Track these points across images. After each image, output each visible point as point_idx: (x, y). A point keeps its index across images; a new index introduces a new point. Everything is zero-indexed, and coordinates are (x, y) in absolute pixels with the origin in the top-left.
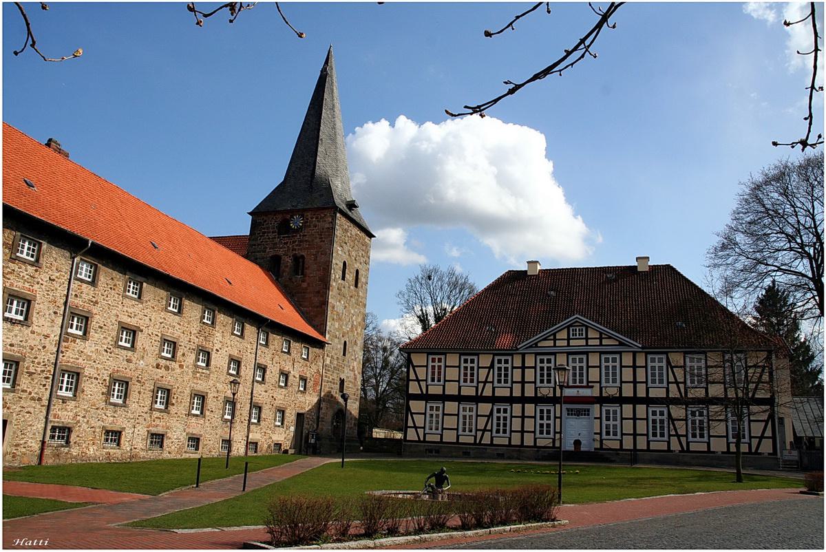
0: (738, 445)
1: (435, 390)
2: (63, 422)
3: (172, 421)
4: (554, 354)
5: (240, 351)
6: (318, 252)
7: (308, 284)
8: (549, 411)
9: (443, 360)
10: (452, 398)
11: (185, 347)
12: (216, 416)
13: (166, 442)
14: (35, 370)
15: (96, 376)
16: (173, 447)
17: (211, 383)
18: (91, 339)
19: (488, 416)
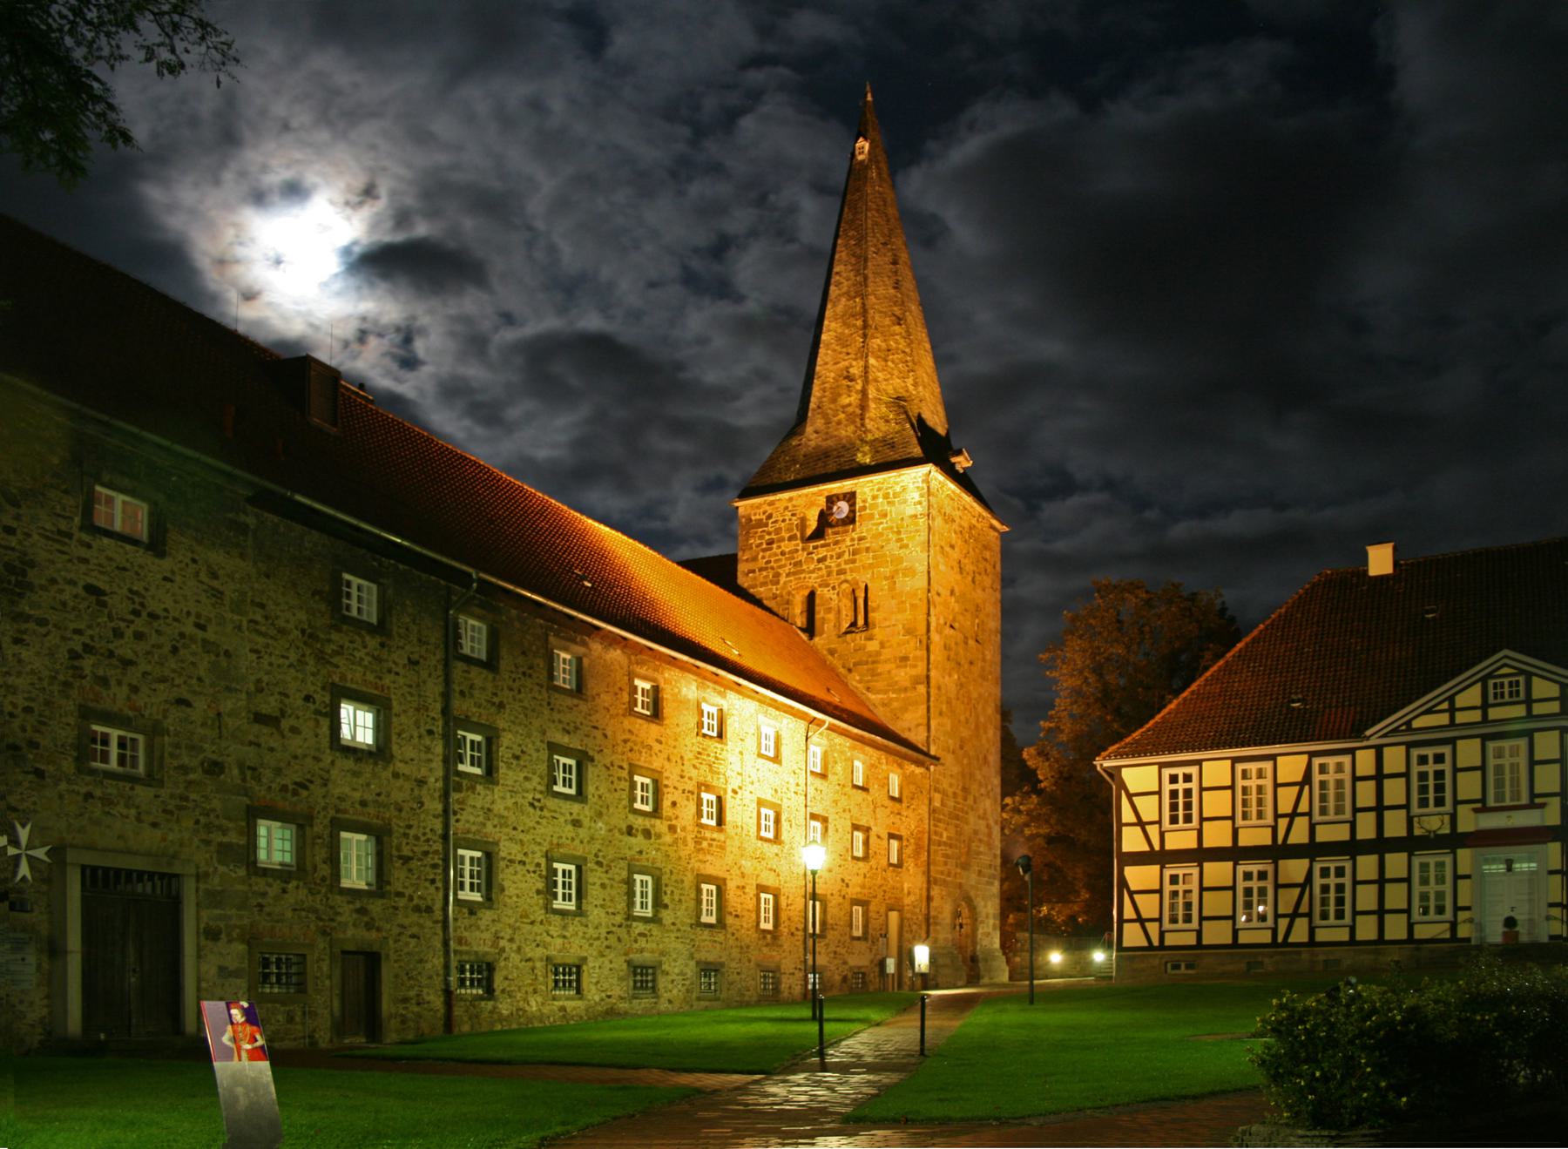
2: (476, 953)
3: (667, 940)
5: (776, 791)
6: (896, 572)
10: (1217, 854)
11: (675, 788)
13: (662, 982)
14: (412, 851)
15: (520, 857)
16: (675, 992)
19: (1302, 886)
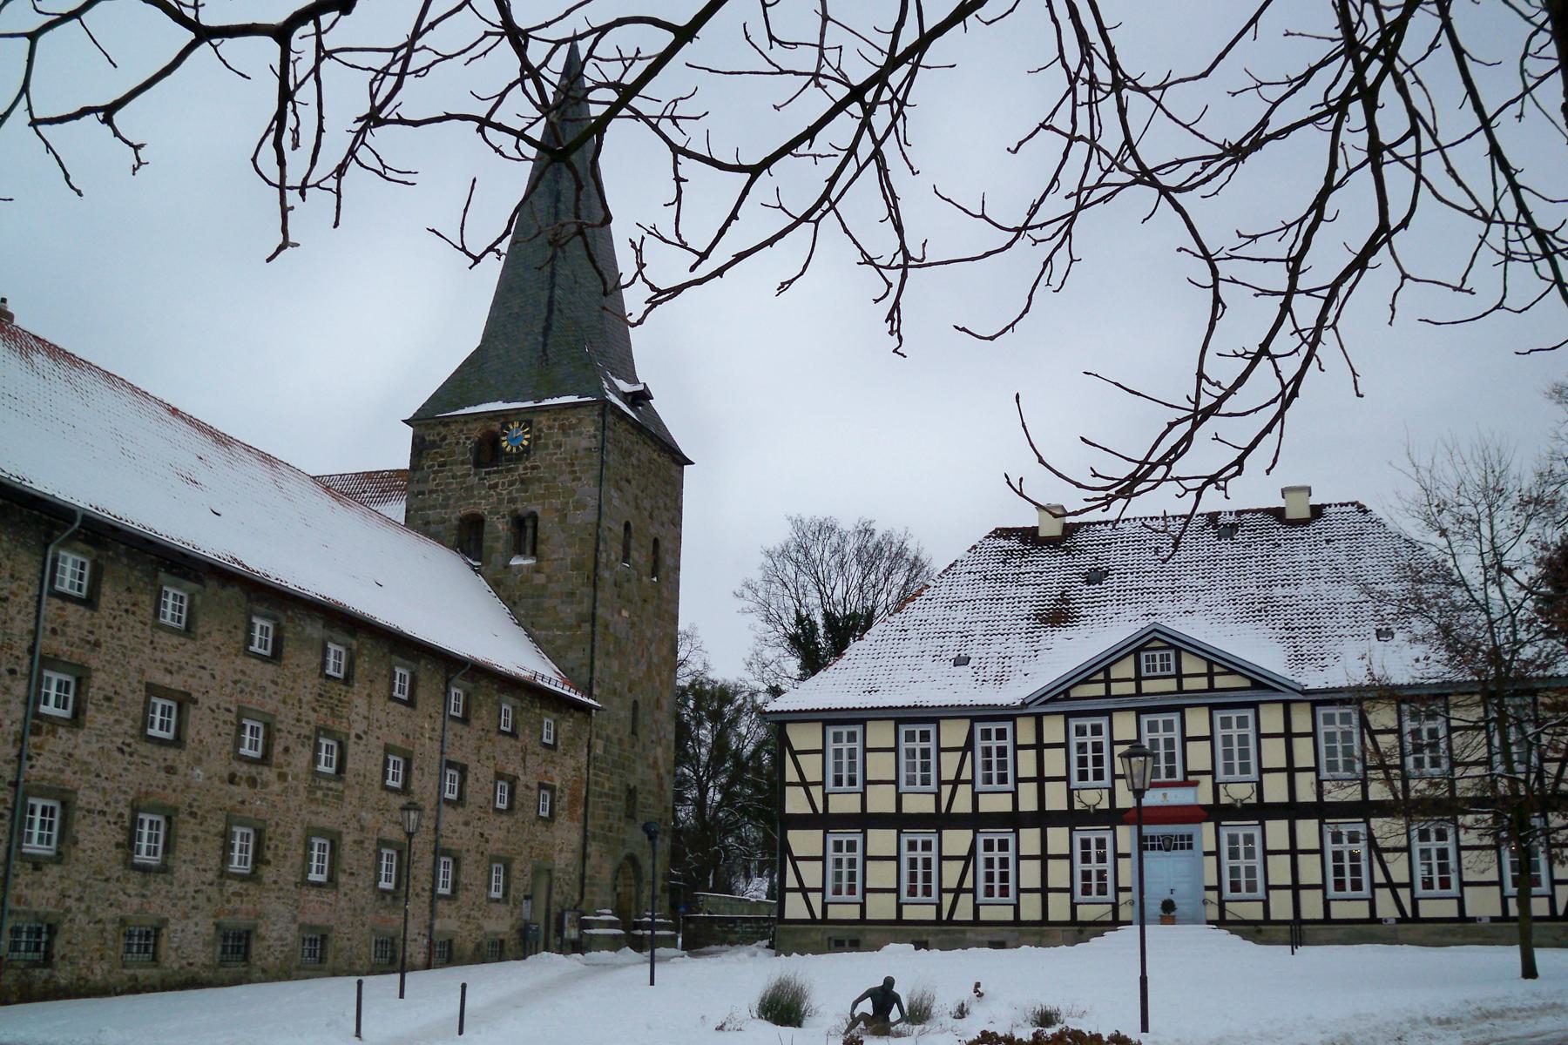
0: (1524, 900)
1: (846, 804)
3: (266, 900)
4: (1108, 713)
5: (407, 736)
8: (1101, 843)
9: (859, 737)
10: (882, 821)
11: (289, 732)
12: (360, 884)
17: (347, 811)
18: (88, 725)
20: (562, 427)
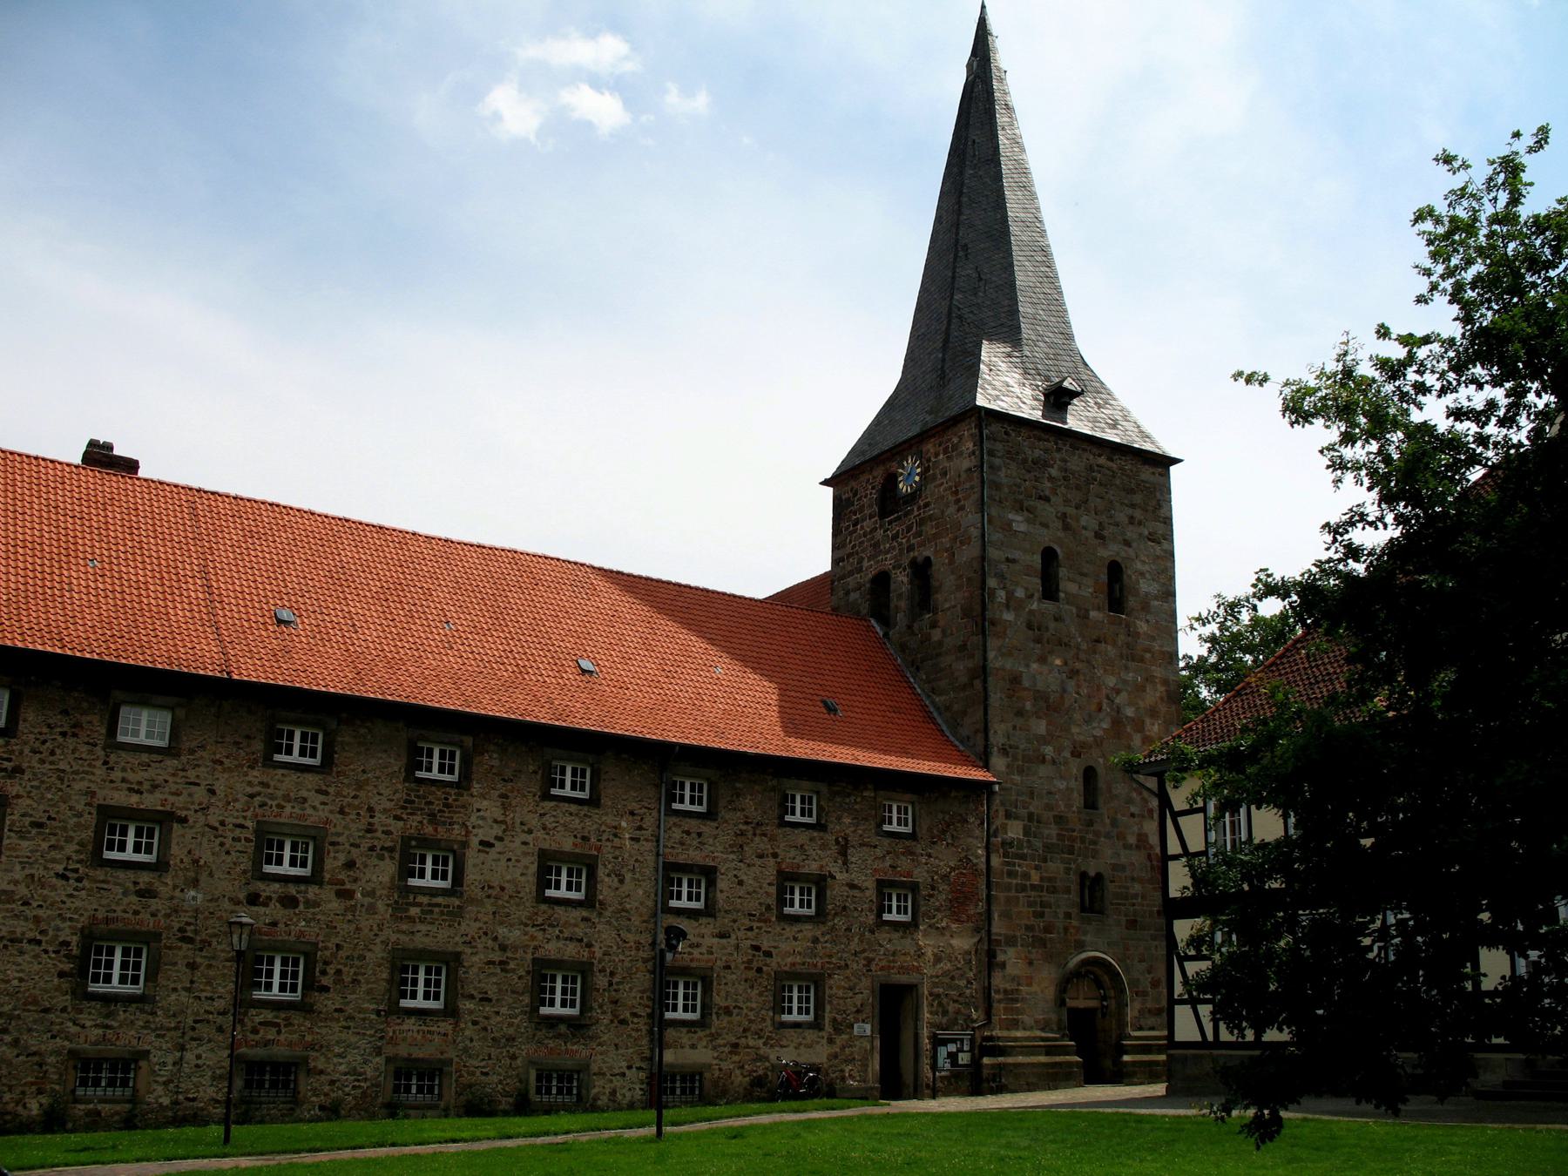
7: (944, 632)
20: (946, 451)
